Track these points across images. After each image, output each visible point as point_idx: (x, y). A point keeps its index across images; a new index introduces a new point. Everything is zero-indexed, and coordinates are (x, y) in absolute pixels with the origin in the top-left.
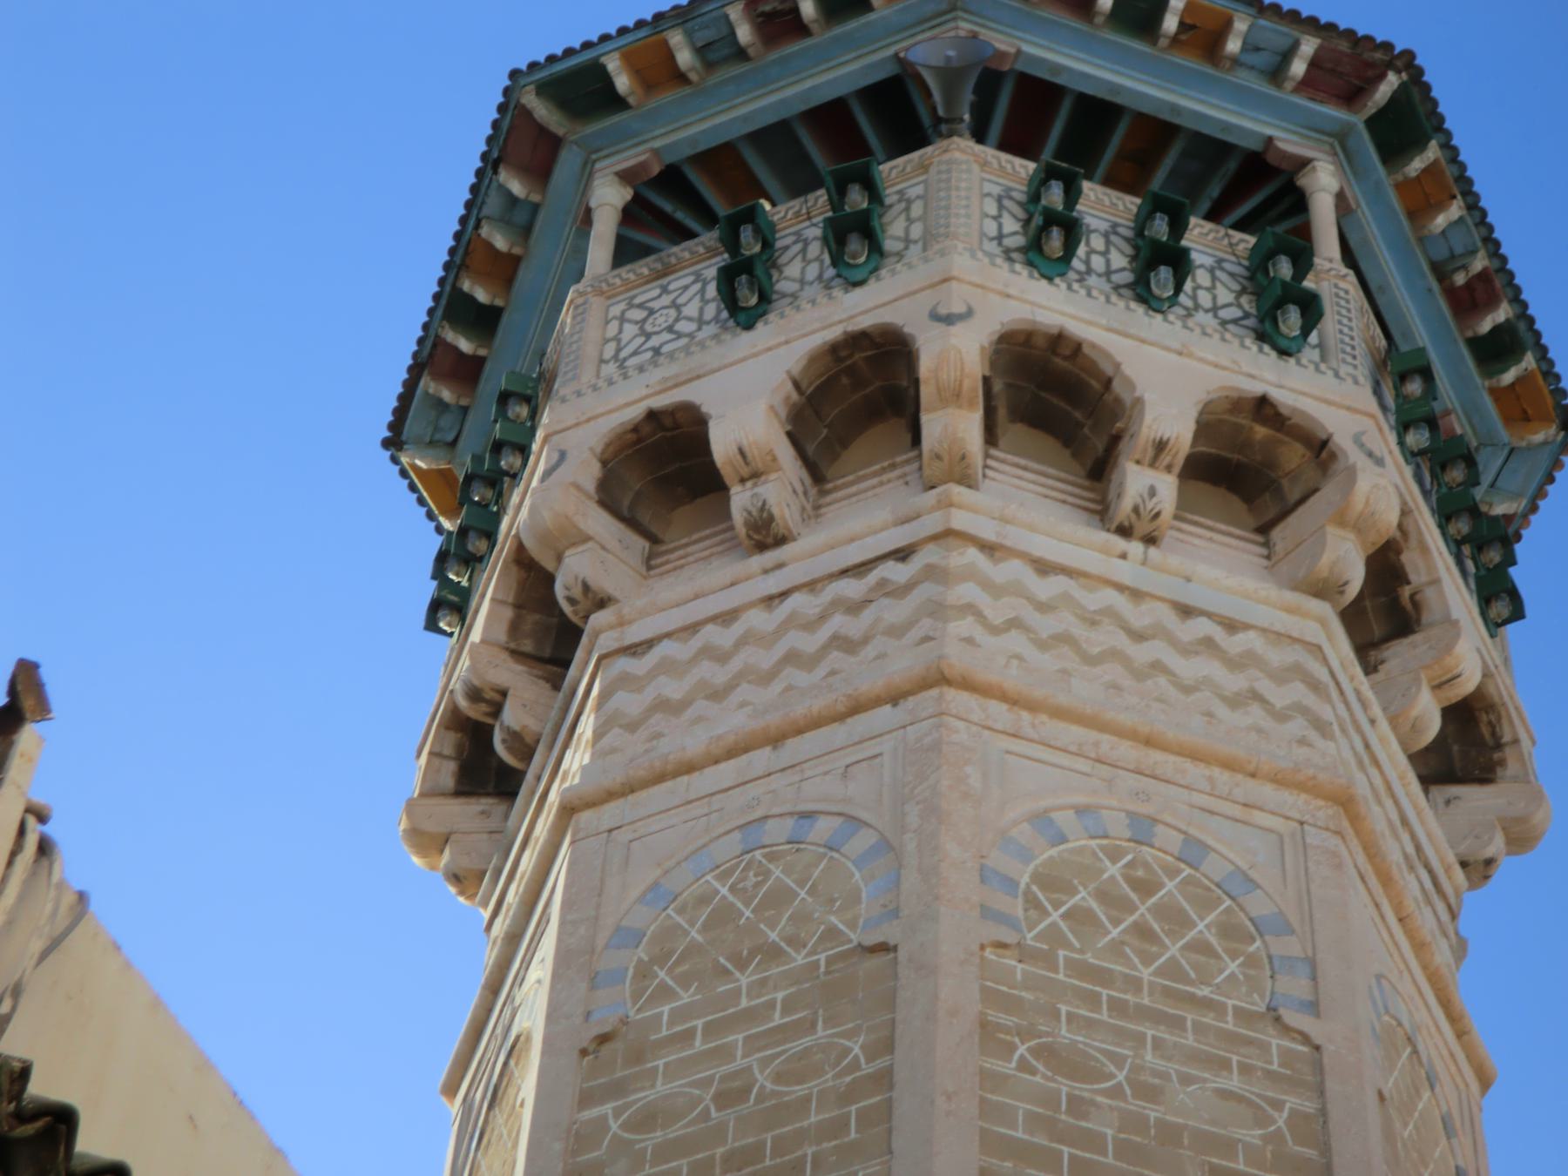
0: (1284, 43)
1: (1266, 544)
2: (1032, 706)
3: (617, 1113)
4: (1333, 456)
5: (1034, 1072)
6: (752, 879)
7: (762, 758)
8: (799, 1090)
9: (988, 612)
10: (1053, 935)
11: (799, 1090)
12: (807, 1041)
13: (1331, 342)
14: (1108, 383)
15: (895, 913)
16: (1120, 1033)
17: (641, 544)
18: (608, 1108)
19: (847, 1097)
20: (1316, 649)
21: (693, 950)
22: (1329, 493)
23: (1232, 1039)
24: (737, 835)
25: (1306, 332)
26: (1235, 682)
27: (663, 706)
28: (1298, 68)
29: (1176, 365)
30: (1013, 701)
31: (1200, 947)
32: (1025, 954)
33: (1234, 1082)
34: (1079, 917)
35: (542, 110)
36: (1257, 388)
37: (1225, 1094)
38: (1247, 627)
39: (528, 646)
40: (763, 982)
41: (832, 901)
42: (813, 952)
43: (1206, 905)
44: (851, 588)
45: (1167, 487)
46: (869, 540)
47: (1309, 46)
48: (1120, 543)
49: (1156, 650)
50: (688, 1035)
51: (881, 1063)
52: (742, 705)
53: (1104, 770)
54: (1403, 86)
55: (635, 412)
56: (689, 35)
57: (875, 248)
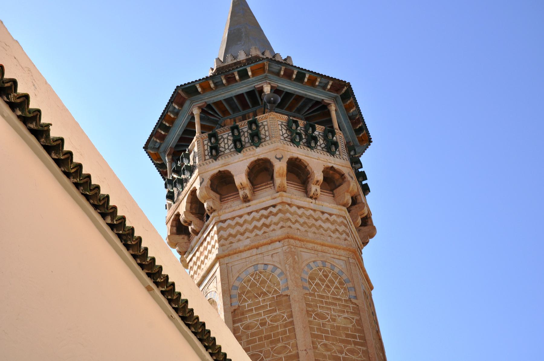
0: (326, 82)
1: (333, 194)
2: (303, 241)
3: (241, 325)
4: (345, 178)
5: (316, 319)
6: (257, 278)
7: (254, 251)
8: (276, 324)
9: (292, 219)
10: (314, 290)
11: (276, 324)
12: (275, 314)
13: (341, 150)
14: (306, 167)
15: (288, 288)
16: (327, 308)
17: (218, 196)
18: (239, 324)
19: (285, 326)
20: (344, 218)
21: (248, 292)
22: (344, 186)
23: (344, 306)
24: (253, 267)
25: (336, 150)
26: (333, 227)
27: (230, 235)
28: (329, 87)
29: (317, 161)
30: (300, 240)
31: (336, 288)
32: (310, 294)
33: (346, 315)
34: (317, 285)
35: (183, 94)
36: (330, 165)
37: (345, 318)
38: (333, 214)
39: (194, 211)
40: (264, 300)
41: (274, 284)
42: (273, 295)
43: (336, 278)
44: (265, 212)
45: (318, 188)
46: (267, 202)
47: (331, 83)
48: (310, 200)
49: (320, 223)
50: (252, 310)
51: (291, 320)
52: (248, 238)
53: (316, 252)
54: (347, 89)
55: (216, 171)
56: (213, 82)
57: (260, 139)
